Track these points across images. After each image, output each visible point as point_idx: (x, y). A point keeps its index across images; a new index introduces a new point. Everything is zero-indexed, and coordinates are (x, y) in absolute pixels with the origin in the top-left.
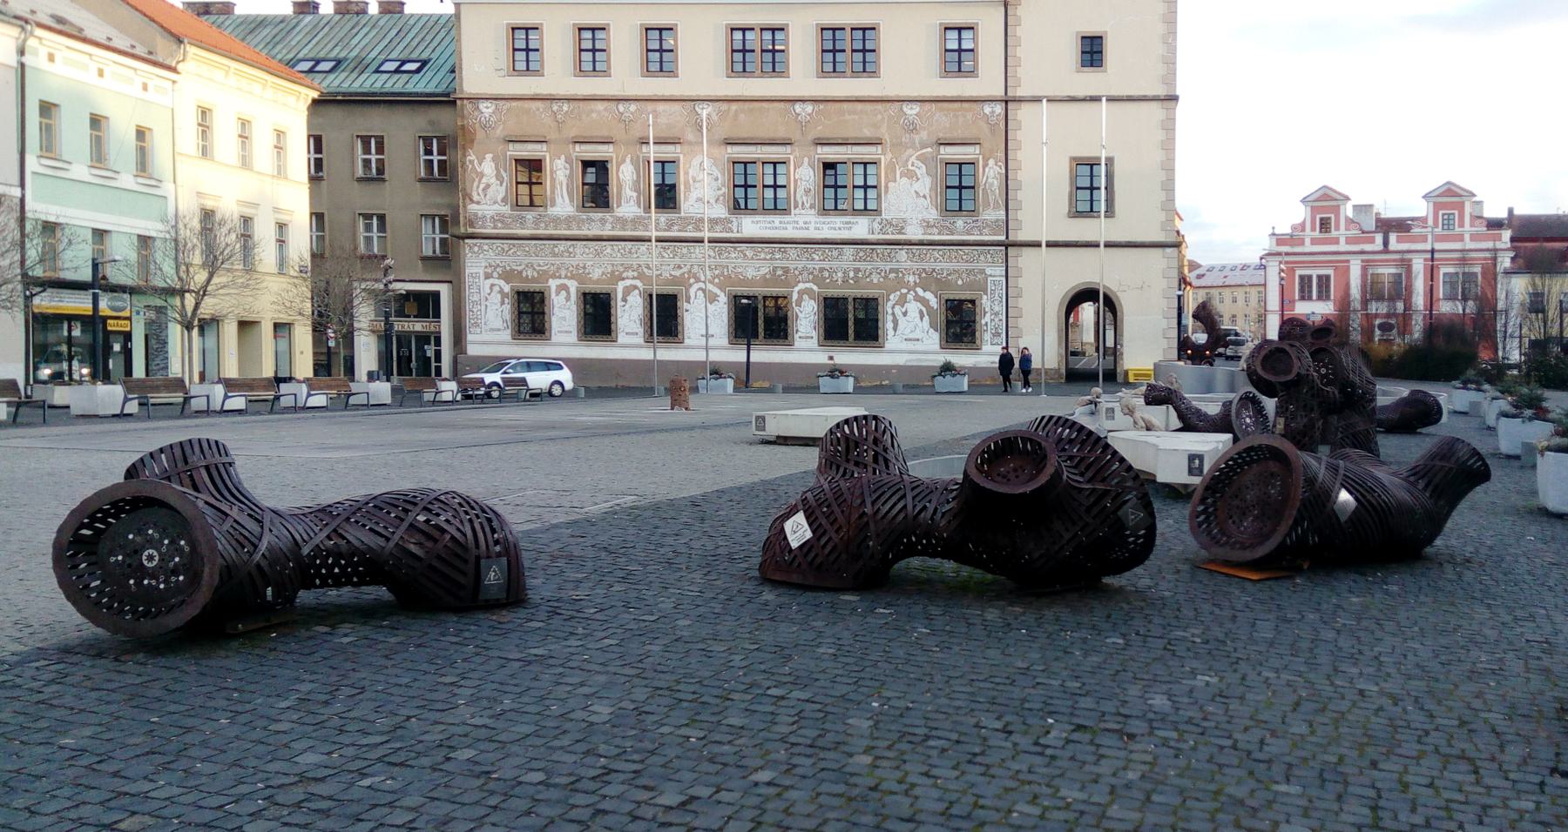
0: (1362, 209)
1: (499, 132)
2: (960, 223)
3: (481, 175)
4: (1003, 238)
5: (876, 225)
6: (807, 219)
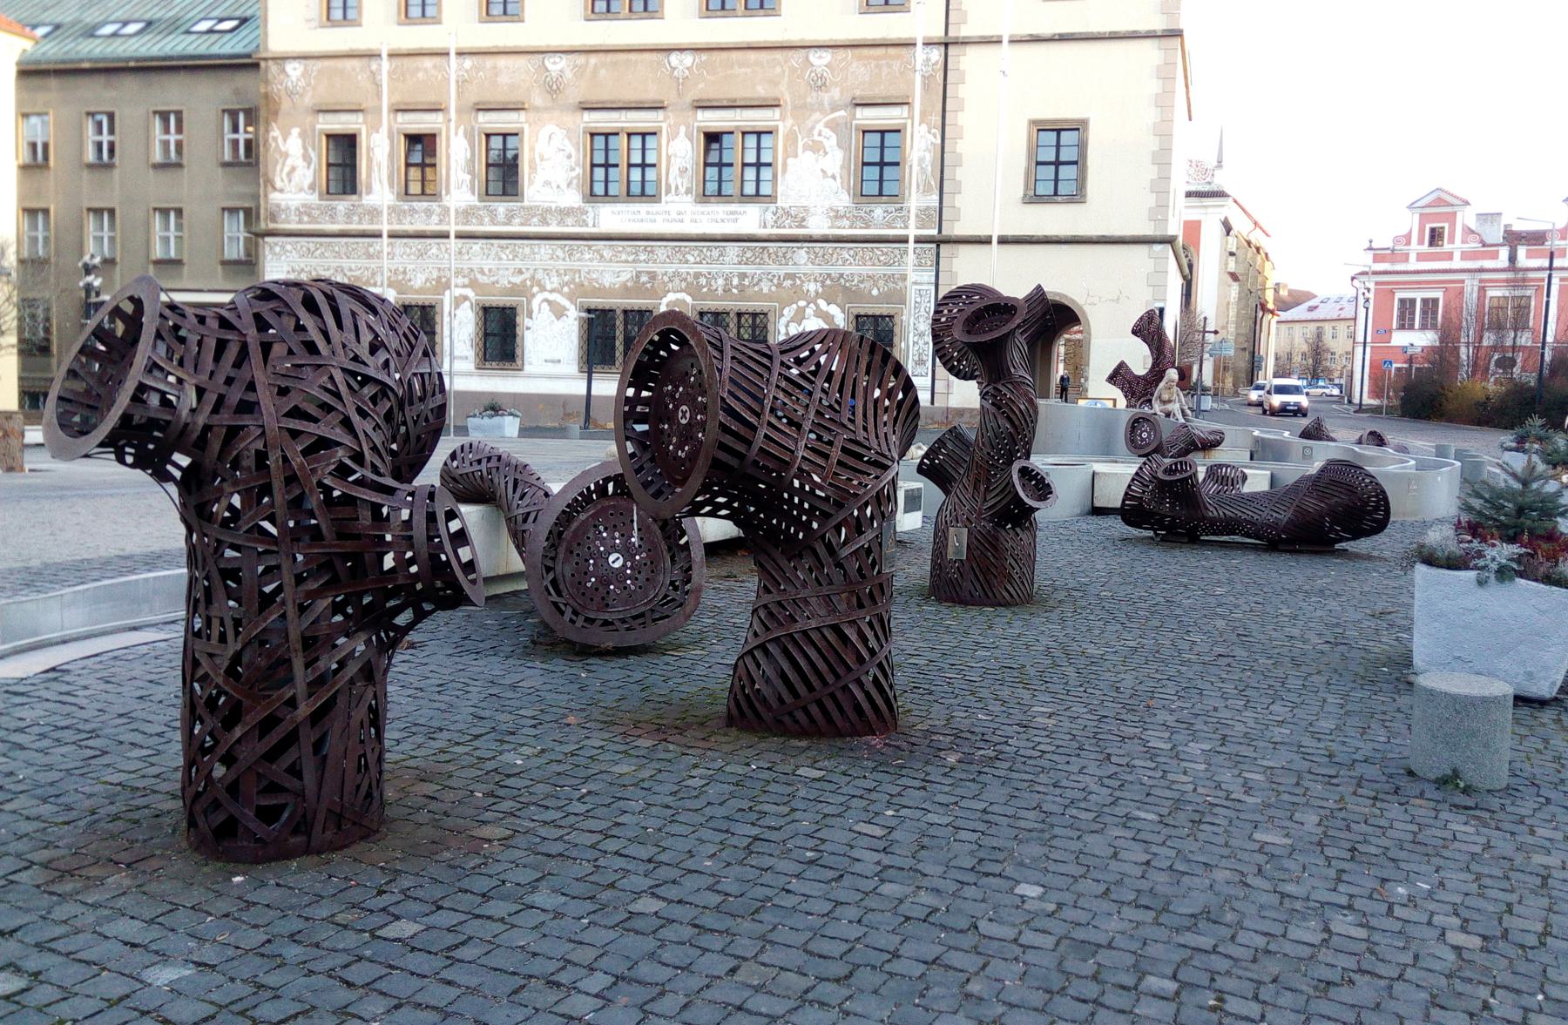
0: (1488, 218)
1: (308, 100)
2: (879, 211)
3: (286, 155)
4: (934, 232)
5: (769, 216)
6: (681, 207)
